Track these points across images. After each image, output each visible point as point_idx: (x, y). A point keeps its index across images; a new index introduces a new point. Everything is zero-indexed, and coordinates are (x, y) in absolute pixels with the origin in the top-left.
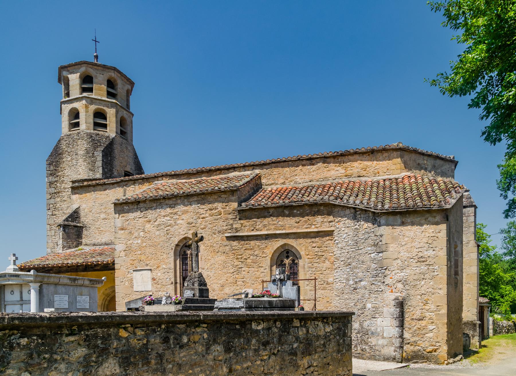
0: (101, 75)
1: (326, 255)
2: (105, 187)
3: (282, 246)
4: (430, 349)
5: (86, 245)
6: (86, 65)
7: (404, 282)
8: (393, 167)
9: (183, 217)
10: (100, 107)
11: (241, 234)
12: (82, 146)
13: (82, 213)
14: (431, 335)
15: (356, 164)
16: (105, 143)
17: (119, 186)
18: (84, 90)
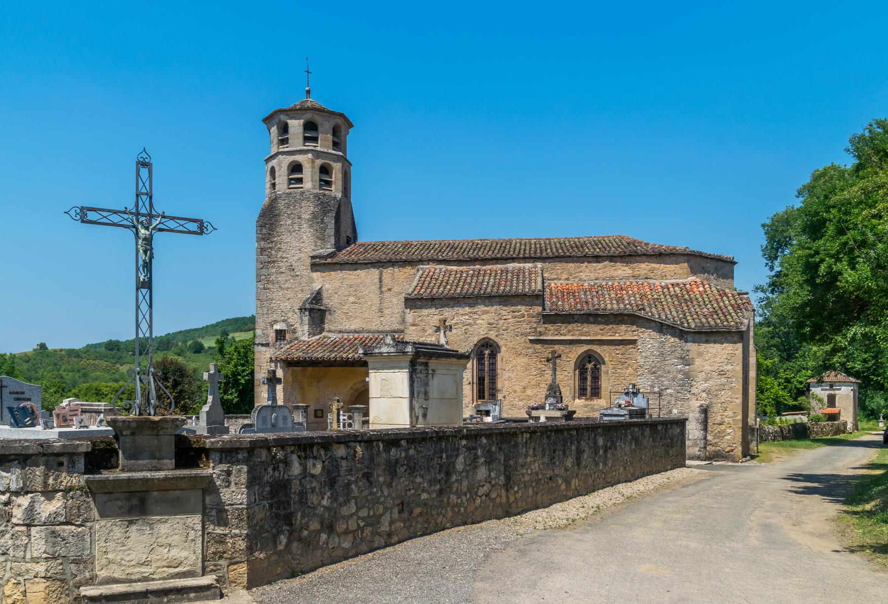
1: (629, 362)
2: (354, 266)
3: (585, 352)
4: (728, 449)
5: (330, 331)
7: (708, 391)
8: (681, 271)
9: (484, 317)
11: (545, 338)
12: (308, 209)
13: (325, 295)
14: (729, 437)
15: (643, 266)
16: (333, 205)
17: (374, 267)
18: (306, 139)
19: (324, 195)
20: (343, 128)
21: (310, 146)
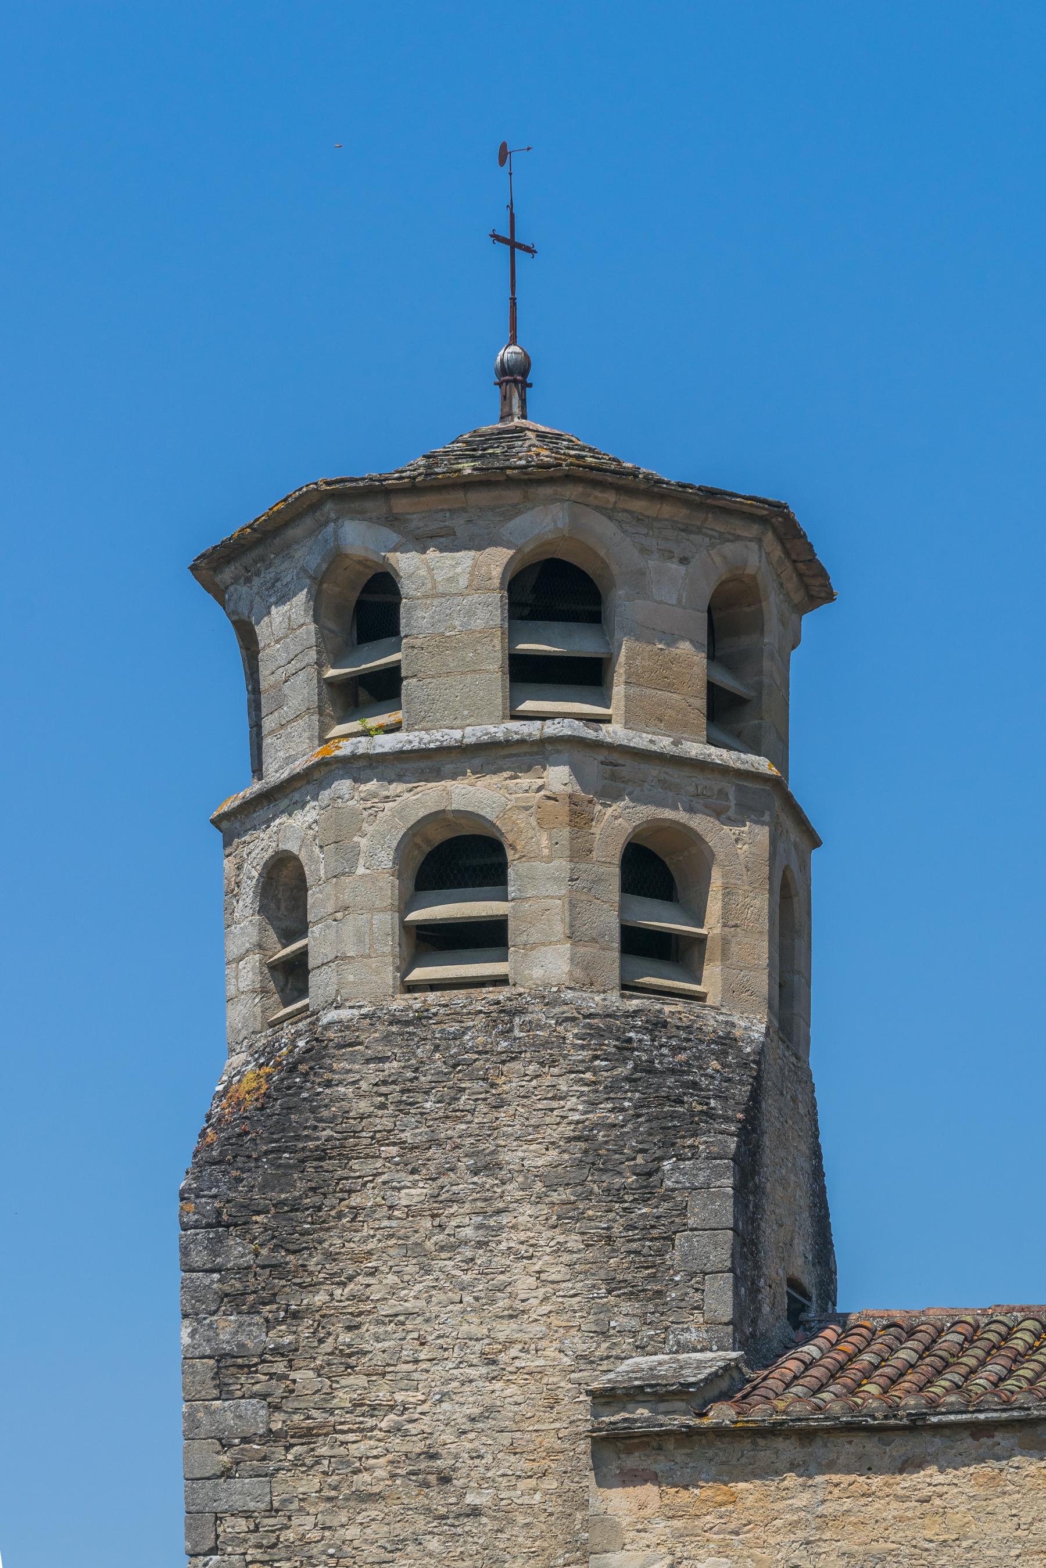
0: (674, 566)
2: (900, 1447)
6: (573, 491)
10: (668, 814)
12: (542, 1117)
18: (527, 673)
19: (657, 1025)
20: (773, 604)
21: (560, 714)
